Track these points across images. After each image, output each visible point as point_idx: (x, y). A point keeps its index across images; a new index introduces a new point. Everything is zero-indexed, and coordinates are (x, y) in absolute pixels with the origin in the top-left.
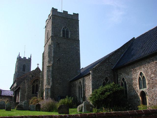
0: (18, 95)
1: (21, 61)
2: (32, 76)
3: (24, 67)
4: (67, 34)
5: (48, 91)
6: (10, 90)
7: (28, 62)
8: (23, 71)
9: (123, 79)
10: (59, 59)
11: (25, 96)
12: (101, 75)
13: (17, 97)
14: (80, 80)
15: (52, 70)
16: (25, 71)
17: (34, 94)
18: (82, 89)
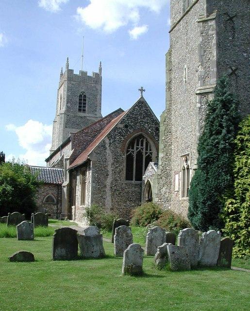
0: (83, 183)
1: (74, 83)
2: (126, 126)
6: (45, 164)
7: (92, 85)
8: (80, 110)
10: (234, 72)
11: (105, 186)
13: (79, 188)
16: (84, 111)
17: (132, 180)
18: (144, 146)
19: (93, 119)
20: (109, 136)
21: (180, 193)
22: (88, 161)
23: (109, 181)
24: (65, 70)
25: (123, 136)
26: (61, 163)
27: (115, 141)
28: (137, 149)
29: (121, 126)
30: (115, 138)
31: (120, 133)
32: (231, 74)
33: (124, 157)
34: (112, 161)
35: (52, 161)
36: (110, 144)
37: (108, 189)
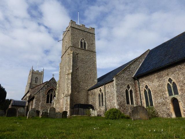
2: (48, 86)
4: (85, 46)
9: (147, 87)
12: (123, 82)
14: (100, 87)
18: (104, 97)
24: (31, 70)
28: (51, 93)
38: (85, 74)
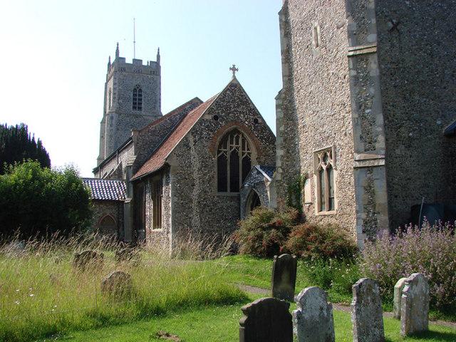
2: (216, 118)
3: (138, 93)
5: (371, 180)
6: (92, 176)
8: (134, 108)
10: (395, 26)
15: (382, 74)
16: (140, 108)
17: (226, 191)
18: (240, 144)
19: (150, 118)
20: (194, 131)
21: (316, 205)
22: (165, 169)
23: (196, 192)
25: (211, 131)
26: (118, 174)
27: (201, 138)
28: (231, 148)
29: (209, 117)
30: (201, 134)
31: (207, 126)
32: (392, 29)
33: (215, 159)
34: (199, 165)
35: (103, 173)
36: (195, 142)
37: (194, 205)
38: (431, 55)
